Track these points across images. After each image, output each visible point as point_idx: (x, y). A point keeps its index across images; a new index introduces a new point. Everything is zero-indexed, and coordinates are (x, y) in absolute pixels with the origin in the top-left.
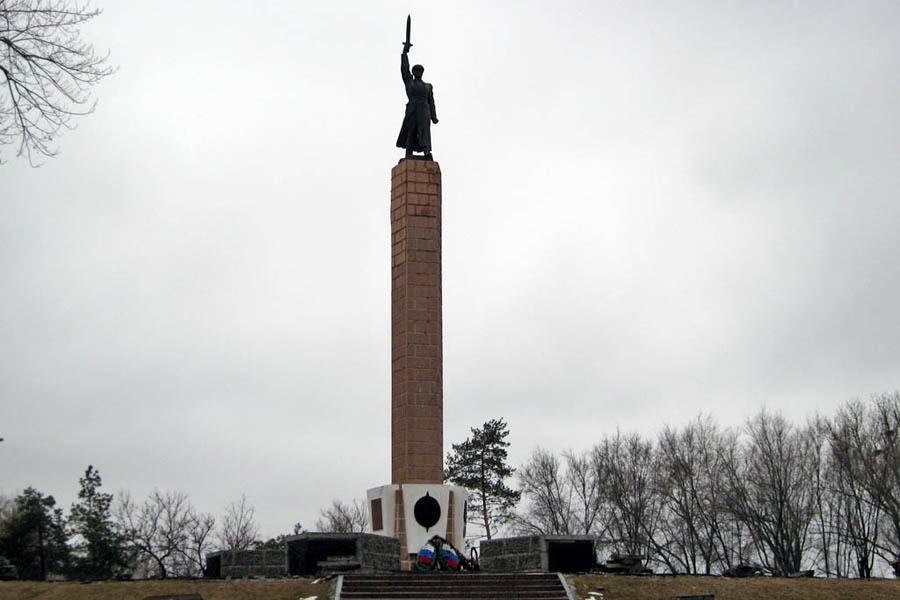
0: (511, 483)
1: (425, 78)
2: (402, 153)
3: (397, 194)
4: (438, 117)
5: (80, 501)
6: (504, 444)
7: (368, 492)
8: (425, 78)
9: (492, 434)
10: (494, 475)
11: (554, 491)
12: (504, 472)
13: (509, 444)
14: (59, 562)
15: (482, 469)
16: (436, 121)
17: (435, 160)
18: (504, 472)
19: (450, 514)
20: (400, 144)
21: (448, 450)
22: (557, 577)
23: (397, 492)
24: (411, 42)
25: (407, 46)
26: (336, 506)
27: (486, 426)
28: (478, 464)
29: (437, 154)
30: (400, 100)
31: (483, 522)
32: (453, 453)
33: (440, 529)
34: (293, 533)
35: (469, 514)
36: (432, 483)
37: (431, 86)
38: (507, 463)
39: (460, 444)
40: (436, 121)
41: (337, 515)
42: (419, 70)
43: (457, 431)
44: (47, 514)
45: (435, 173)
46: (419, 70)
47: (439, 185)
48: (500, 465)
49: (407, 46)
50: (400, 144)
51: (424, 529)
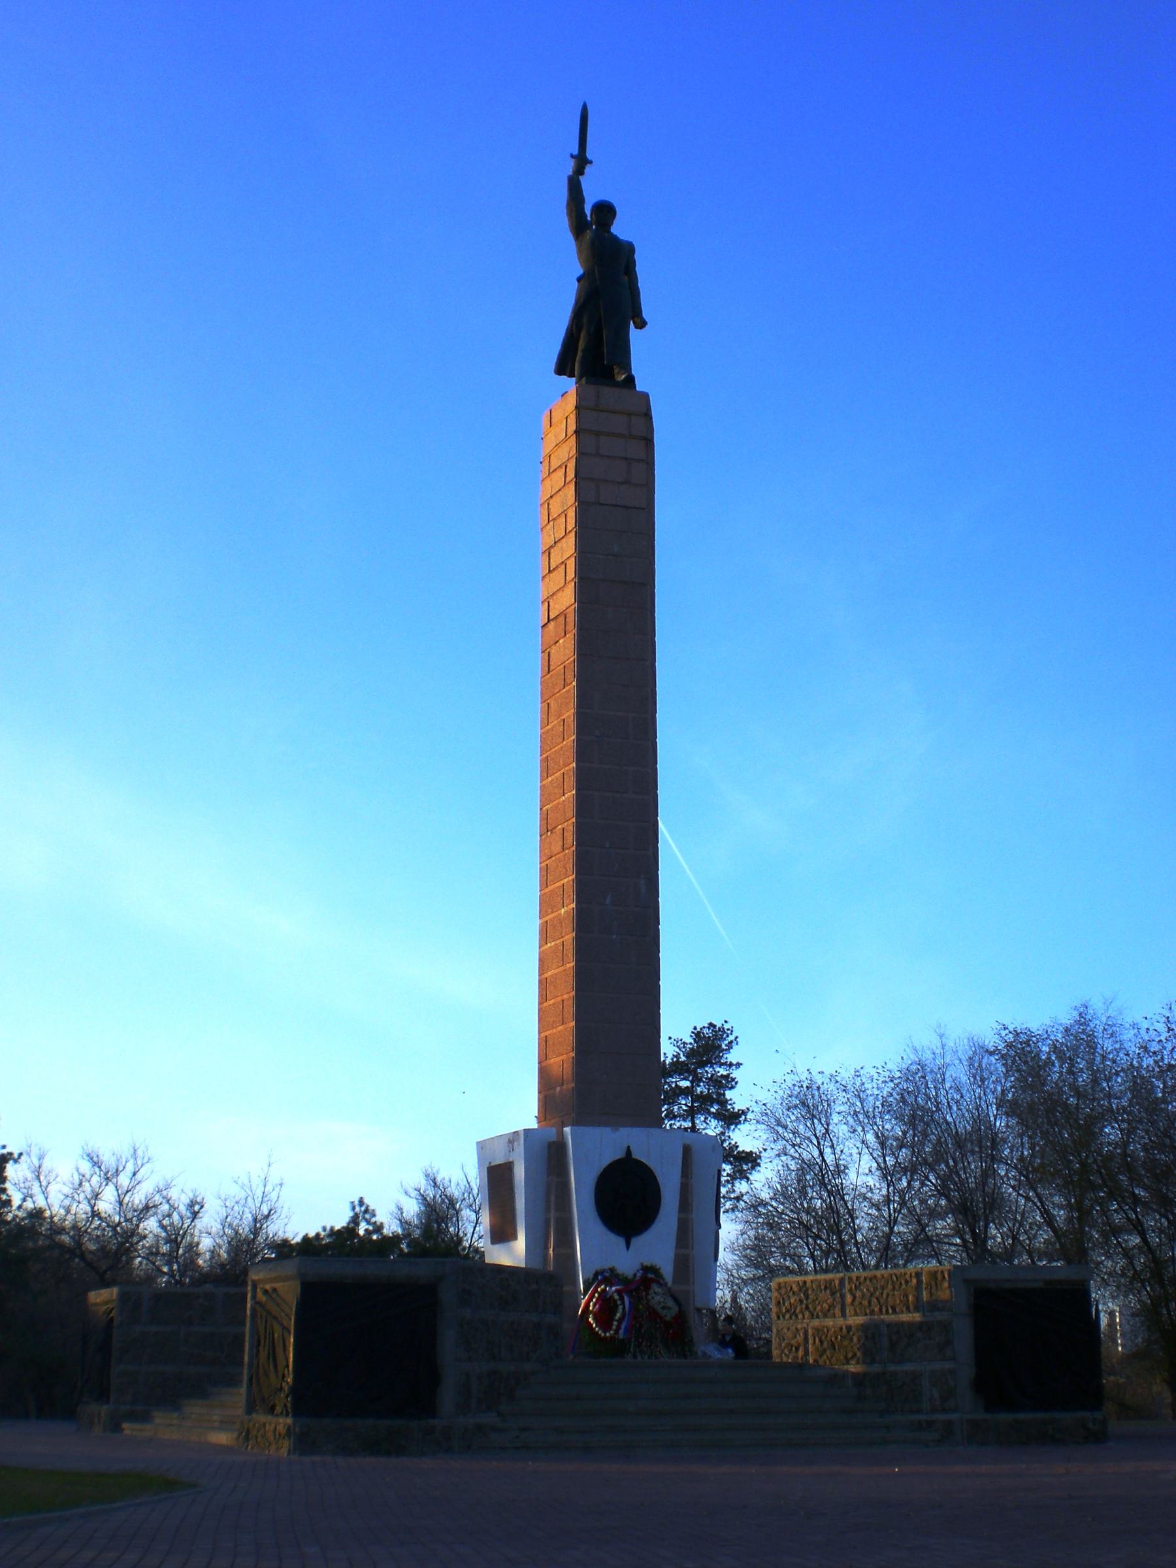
0: (744, 1138)
1: (620, 229)
2: (569, 384)
3: (555, 463)
6: (731, 1065)
7: (481, 1146)
10: (714, 1123)
11: (827, 1151)
12: (732, 1118)
13: (739, 1065)
15: (691, 1113)
16: (641, 324)
17: (640, 387)
18: (732, 1118)
19: (685, 1204)
23: (551, 1145)
25: (582, 161)
26: (427, 1176)
33: (656, 1247)
37: (630, 249)
38: (737, 1098)
40: (641, 324)
41: (430, 1193)
42: (605, 211)
44: (1013, 1121)
45: (643, 411)
46: (605, 211)
47: (648, 441)
48: (723, 1102)
49: (582, 161)
50: (563, 368)
51: (636, 1155)
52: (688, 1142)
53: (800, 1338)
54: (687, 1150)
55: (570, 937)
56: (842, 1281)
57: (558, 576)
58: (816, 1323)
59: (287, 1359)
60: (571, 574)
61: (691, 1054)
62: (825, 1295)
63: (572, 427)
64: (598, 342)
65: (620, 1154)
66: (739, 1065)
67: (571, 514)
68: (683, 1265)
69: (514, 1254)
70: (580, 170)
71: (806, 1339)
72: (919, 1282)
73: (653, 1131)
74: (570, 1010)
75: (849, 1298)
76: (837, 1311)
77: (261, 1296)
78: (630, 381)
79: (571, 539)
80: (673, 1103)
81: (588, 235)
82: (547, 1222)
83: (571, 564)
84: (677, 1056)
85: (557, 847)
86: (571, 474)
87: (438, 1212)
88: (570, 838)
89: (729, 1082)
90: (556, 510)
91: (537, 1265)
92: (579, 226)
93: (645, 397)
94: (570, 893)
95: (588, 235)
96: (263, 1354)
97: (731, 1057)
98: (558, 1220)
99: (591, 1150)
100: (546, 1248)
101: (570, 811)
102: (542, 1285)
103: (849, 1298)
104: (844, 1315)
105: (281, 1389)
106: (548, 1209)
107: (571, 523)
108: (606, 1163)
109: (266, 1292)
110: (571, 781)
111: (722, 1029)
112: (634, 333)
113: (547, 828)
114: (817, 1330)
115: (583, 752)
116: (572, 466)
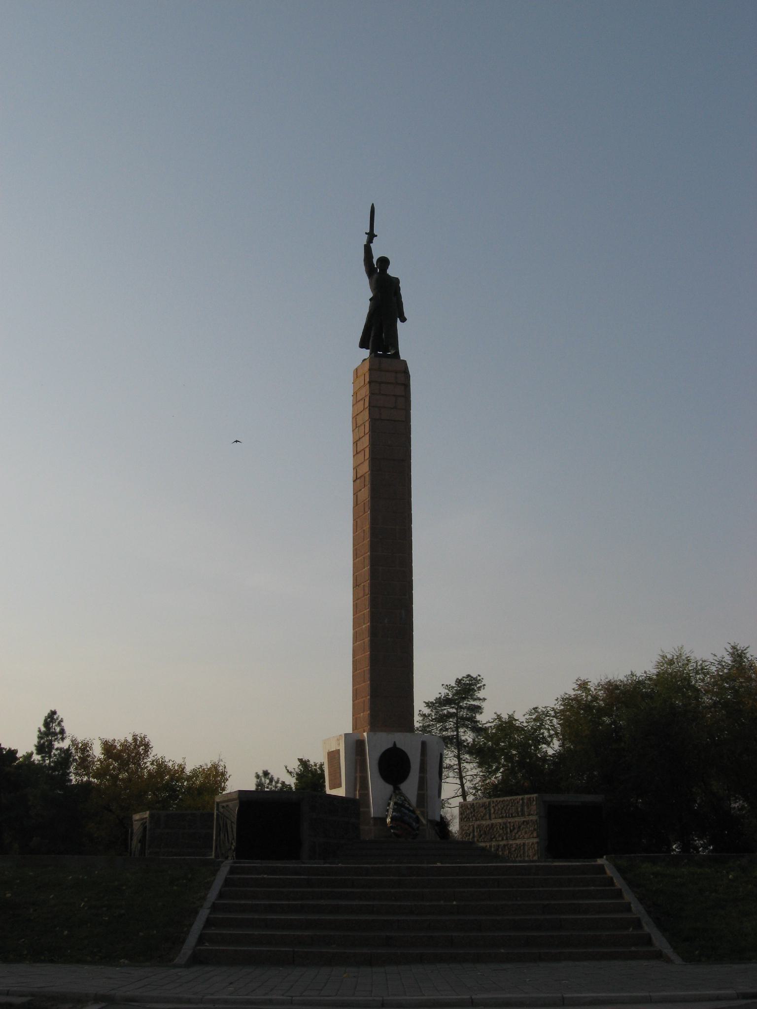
1: (391, 272)
2: (366, 353)
3: (359, 397)
4: (406, 315)
5: (97, 752)
8: (391, 272)
9: (467, 688)
13: (484, 699)
14: (452, 812)
16: (404, 320)
19: (423, 769)
20: (363, 344)
21: (419, 706)
22: (601, 869)
24: (375, 232)
25: (371, 236)
27: (459, 682)
28: (451, 724)
29: (405, 352)
30: (360, 297)
31: (458, 781)
32: (427, 711)
34: (252, 787)
35: (445, 773)
36: (400, 731)
39: (432, 700)
40: (404, 320)
42: (384, 262)
43: (429, 683)
46: (384, 262)
47: (406, 386)
49: (371, 236)
50: (363, 344)
51: (398, 746)
52: (424, 739)
53: (471, 829)
54: (424, 744)
55: (367, 640)
56: (489, 803)
57: (361, 456)
58: (478, 822)
59: (244, 863)
60: (367, 456)
61: (457, 693)
62: (482, 809)
63: (367, 380)
64: (381, 328)
65: (390, 745)
66: (484, 699)
67: (367, 424)
68: (422, 799)
69: (341, 792)
70: (370, 240)
71: (473, 831)
72: (523, 802)
73: (408, 734)
74: (367, 676)
75: (492, 811)
76: (487, 816)
77: (221, 810)
78: (397, 355)
79: (367, 437)
80: (446, 721)
81: (375, 276)
82: (356, 778)
83: (367, 450)
84: (448, 694)
85: (361, 595)
86: (367, 404)
87: (310, 777)
88: (367, 590)
89: (477, 709)
90: (360, 422)
91: (351, 796)
92: (370, 269)
93: (404, 362)
94: (367, 618)
95: (375, 276)
96: (222, 836)
97: (480, 694)
98: (360, 777)
99: (376, 745)
100: (355, 790)
101: (367, 577)
102: (351, 807)
103: (492, 811)
104: (490, 819)
105: (231, 849)
106: (356, 773)
107: (367, 430)
108: (383, 750)
109: (223, 807)
110: (367, 561)
111: (475, 679)
112: (399, 324)
113: (356, 585)
114: (479, 826)
115: (373, 547)
116: (367, 399)
